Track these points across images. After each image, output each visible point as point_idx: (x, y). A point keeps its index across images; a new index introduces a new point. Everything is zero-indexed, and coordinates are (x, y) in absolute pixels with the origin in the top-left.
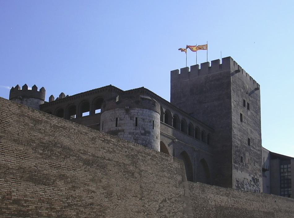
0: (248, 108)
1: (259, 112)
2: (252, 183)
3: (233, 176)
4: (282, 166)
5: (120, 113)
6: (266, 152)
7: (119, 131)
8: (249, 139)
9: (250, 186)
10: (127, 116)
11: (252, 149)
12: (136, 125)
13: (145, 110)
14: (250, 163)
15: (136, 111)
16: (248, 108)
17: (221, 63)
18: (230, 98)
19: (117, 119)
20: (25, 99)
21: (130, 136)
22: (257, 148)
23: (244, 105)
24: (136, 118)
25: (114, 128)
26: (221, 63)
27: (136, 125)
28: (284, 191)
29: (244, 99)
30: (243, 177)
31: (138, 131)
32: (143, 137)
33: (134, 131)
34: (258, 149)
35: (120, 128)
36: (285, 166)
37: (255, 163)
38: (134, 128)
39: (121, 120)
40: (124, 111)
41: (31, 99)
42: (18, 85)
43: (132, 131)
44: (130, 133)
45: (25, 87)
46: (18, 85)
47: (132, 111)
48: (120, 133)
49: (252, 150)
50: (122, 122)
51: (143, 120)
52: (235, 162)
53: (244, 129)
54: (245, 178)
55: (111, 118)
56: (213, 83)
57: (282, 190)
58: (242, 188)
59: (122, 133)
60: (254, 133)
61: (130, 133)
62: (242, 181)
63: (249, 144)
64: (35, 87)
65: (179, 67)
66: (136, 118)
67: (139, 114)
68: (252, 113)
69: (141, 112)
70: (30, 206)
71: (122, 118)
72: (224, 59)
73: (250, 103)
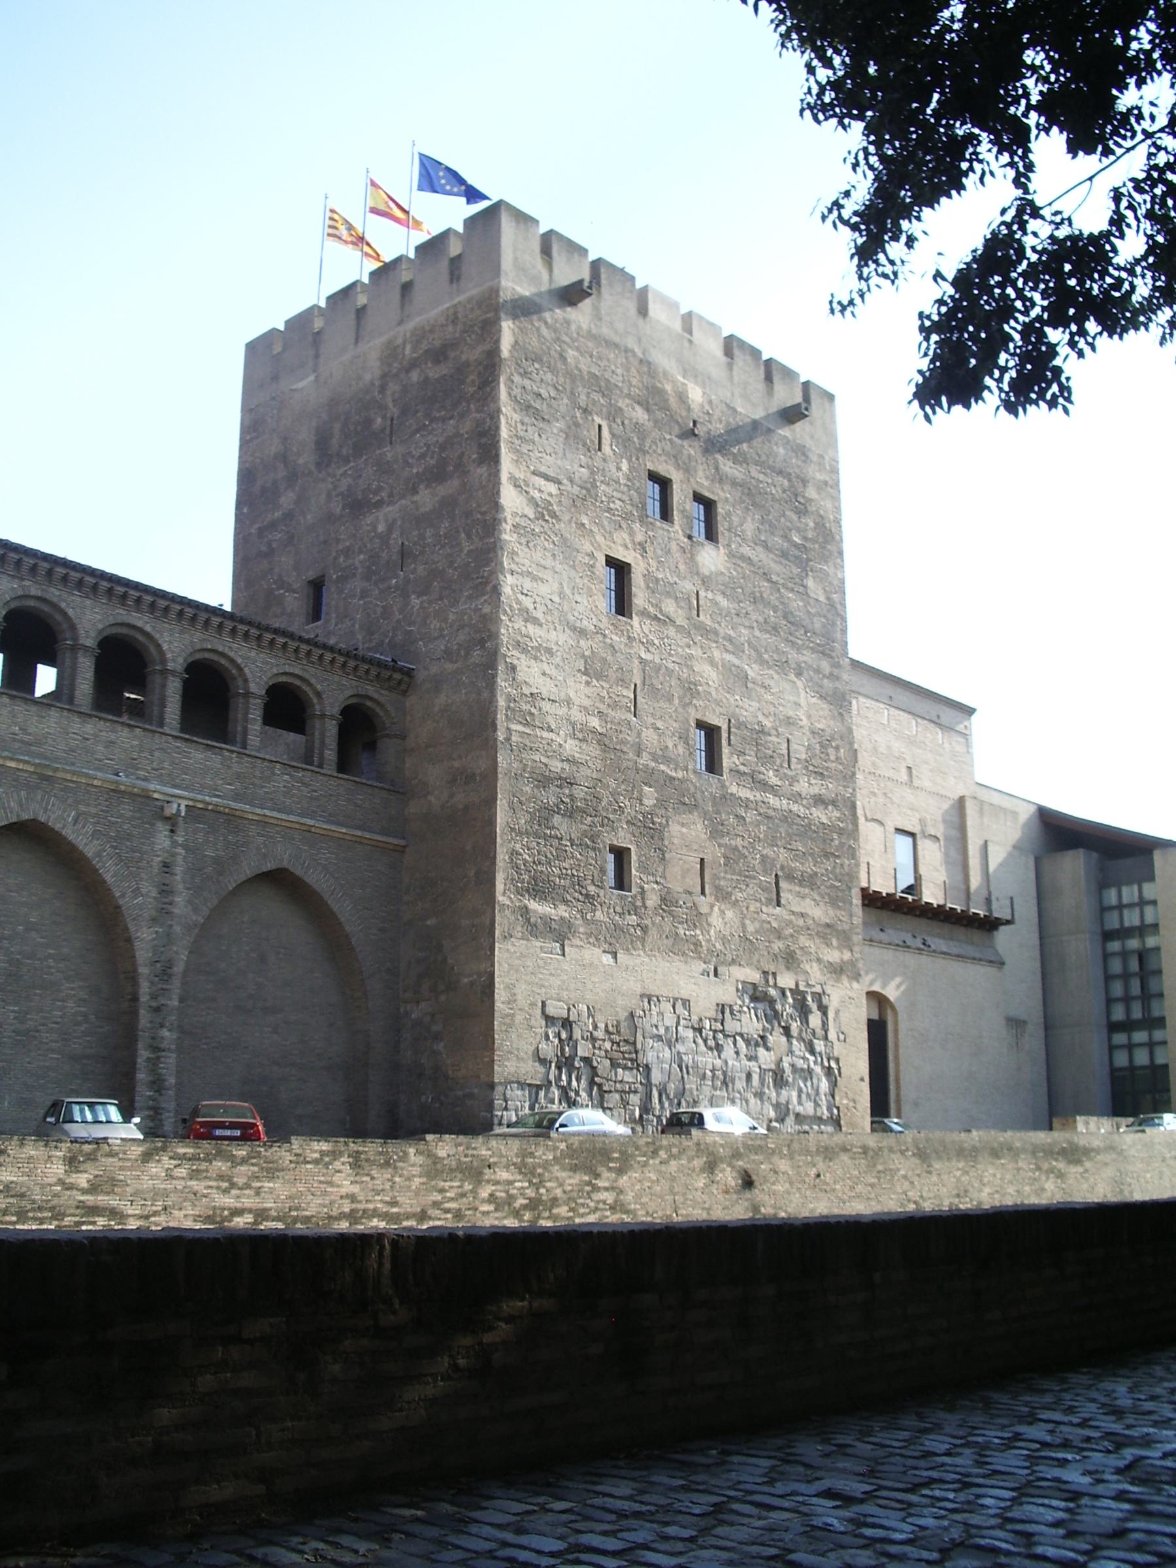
1: (825, 559)
2: (751, 1024)
3: (509, 987)
4: (1111, 896)
6: (998, 810)
8: (711, 733)
9: (719, 1048)
11: (745, 793)
14: (718, 888)
18: (490, 456)
22: (806, 786)
28: (1130, 1047)
29: (650, 466)
30: (639, 991)
34: (815, 790)
36: (1125, 890)
37: (783, 885)
42: (974, 710)
46: (974, 710)
49: (746, 803)
53: (642, 661)
54: (654, 989)
56: (415, 376)
57: (1120, 1038)
58: (614, 1065)
60: (766, 687)
62: (623, 1015)
63: (713, 764)
68: (743, 558)
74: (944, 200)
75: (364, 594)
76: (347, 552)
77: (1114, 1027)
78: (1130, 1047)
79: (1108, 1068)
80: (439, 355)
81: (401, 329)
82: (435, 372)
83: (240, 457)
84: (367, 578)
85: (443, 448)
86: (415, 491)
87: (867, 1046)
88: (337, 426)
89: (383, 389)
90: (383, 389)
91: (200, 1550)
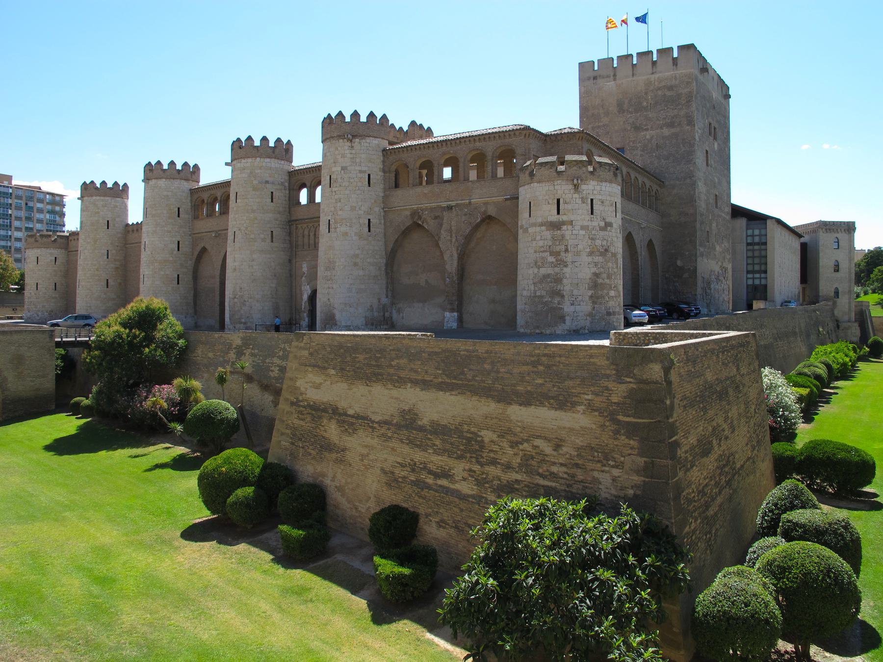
0: (715, 138)
5: (563, 189)
7: (563, 223)
10: (576, 196)
12: (592, 213)
13: (604, 184)
15: (591, 187)
16: (715, 138)
17: (675, 55)
19: (558, 201)
20: (357, 140)
21: (582, 232)
23: (710, 134)
24: (592, 200)
25: (554, 217)
26: (675, 55)
27: (592, 213)
31: (595, 224)
32: (602, 233)
33: (590, 223)
35: (565, 218)
38: (588, 217)
39: (566, 203)
40: (571, 187)
41: (368, 140)
43: (586, 223)
44: (583, 228)
45: (355, 115)
47: (584, 187)
48: (564, 227)
50: (570, 207)
51: (602, 202)
52: (701, 245)
55: (547, 197)
56: (660, 93)
57: (750, 276)
59: (570, 227)
61: (583, 228)
64: (372, 115)
65: (595, 55)
66: (592, 200)
67: (595, 192)
69: (598, 188)
70: (706, 490)
71: (568, 200)
72: (681, 48)
73: (717, 126)
74: (872, 249)
75: (641, 156)
76: (634, 142)
77: (748, 272)
78: (753, 278)
79: (209, 546)
80: (670, 88)
81: (653, 76)
82: (669, 93)
83: (844, 222)
84: (643, 151)
85: (673, 118)
86: (661, 128)
87: (103, 453)
88: (626, 101)
89: (646, 93)
90: (646, 93)
91: (500, 480)
